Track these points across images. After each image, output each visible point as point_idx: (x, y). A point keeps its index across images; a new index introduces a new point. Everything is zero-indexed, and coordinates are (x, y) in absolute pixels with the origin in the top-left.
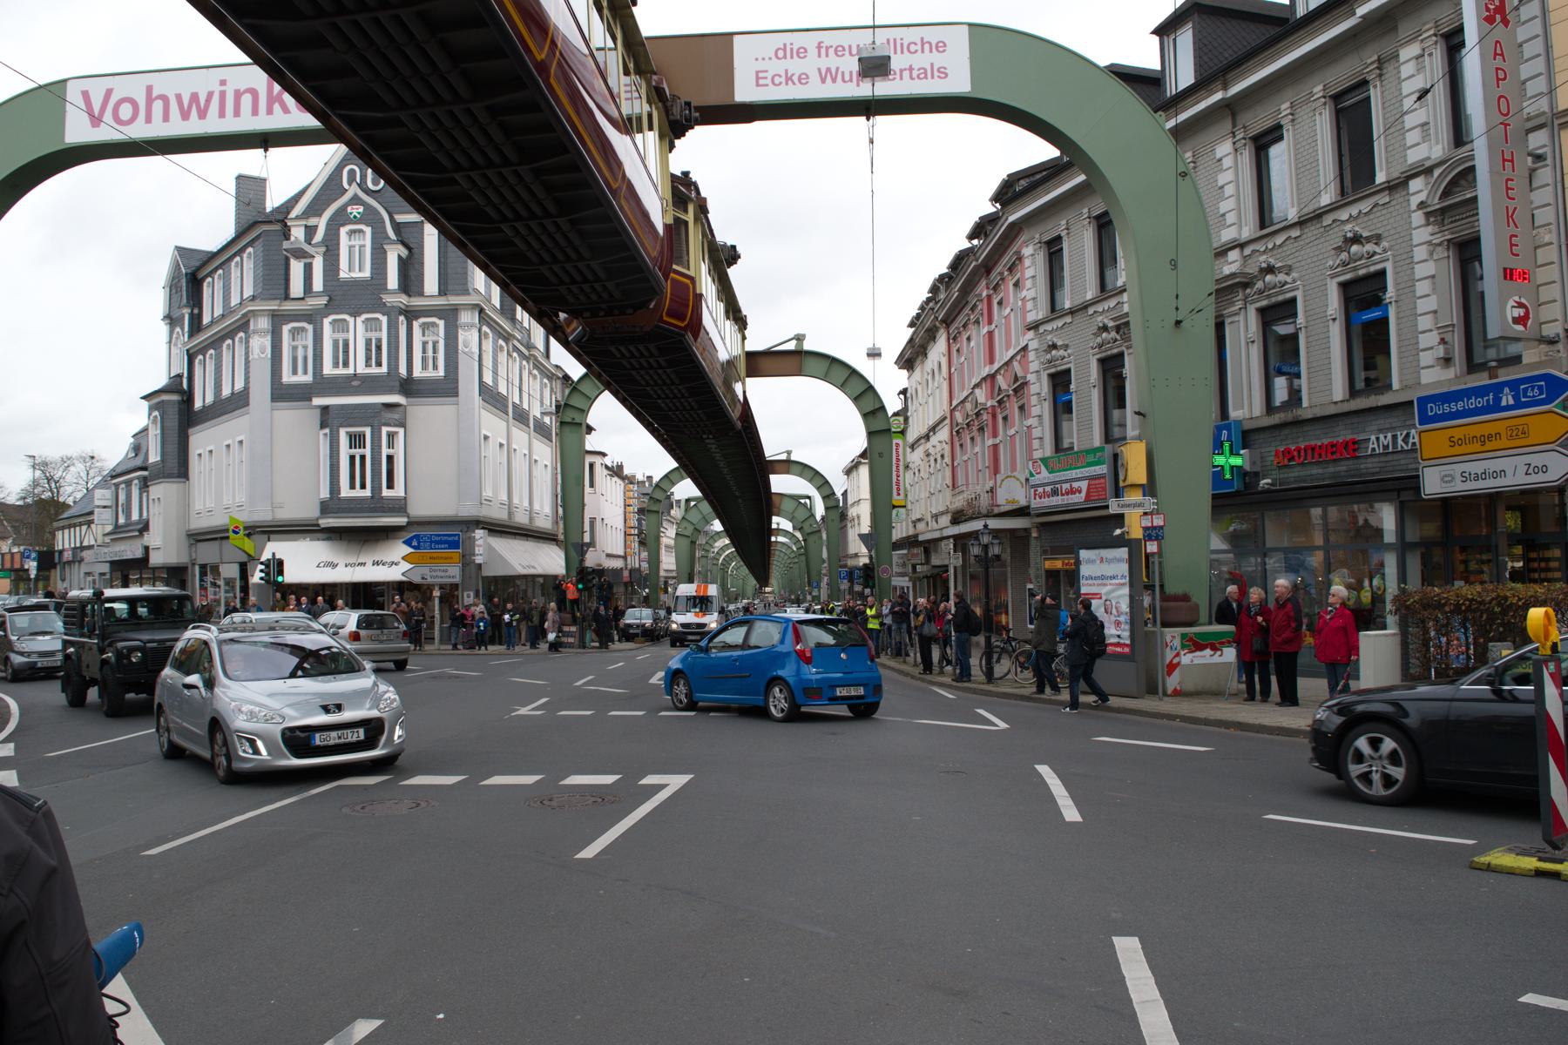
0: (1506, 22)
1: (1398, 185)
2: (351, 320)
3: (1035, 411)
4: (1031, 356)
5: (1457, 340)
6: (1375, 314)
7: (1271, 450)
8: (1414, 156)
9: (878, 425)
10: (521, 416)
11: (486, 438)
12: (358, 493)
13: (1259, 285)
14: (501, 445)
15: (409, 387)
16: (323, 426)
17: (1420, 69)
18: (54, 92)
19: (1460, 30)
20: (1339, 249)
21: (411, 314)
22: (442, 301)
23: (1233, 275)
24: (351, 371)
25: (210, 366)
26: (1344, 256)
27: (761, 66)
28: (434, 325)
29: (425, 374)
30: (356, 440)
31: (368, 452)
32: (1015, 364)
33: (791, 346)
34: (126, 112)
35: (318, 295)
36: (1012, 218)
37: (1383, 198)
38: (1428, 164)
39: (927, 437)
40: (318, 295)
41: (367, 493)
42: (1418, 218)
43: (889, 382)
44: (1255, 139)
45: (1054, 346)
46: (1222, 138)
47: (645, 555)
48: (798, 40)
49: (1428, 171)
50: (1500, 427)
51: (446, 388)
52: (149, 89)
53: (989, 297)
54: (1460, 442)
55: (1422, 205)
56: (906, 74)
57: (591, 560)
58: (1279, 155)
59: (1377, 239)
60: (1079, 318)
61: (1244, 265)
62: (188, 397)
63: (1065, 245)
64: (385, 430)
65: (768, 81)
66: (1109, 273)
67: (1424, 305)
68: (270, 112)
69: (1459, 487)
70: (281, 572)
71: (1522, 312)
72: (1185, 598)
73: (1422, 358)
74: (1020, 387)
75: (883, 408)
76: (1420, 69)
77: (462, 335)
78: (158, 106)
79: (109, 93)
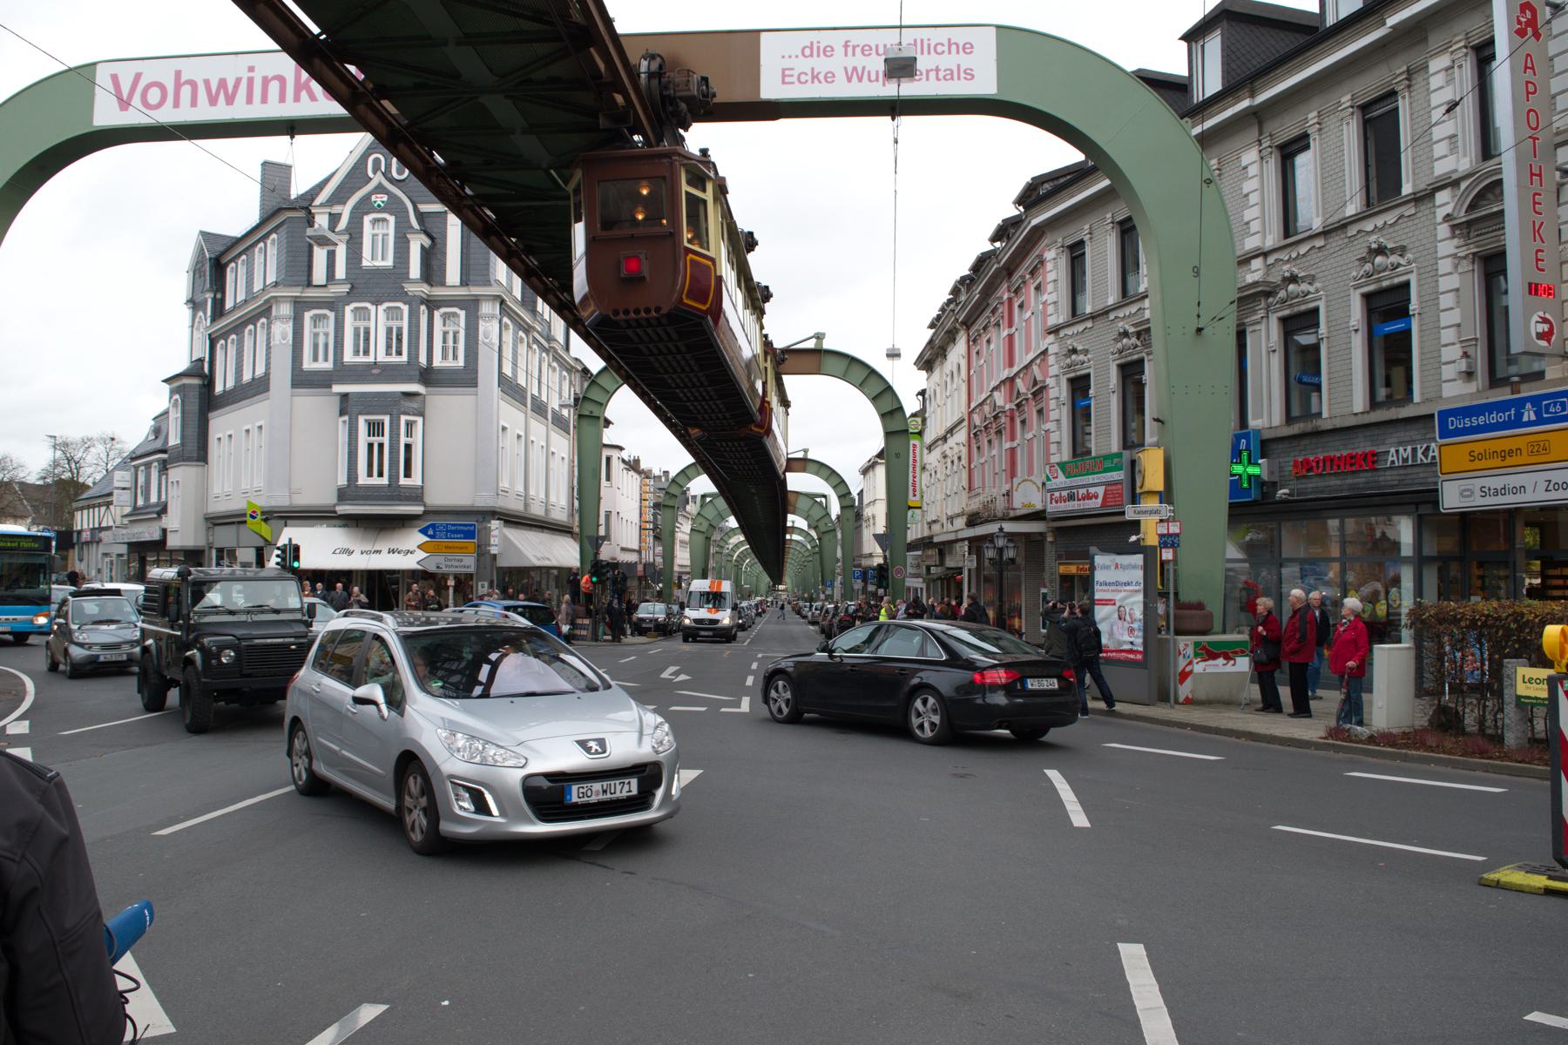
0: (1537, 36)
1: (1424, 197)
2: (372, 308)
3: (1053, 415)
4: (1051, 360)
5: (1480, 355)
6: (1397, 326)
7: (1288, 460)
8: (1440, 169)
9: (896, 425)
10: (539, 408)
11: (504, 429)
12: (375, 481)
13: (1282, 294)
14: (519, 437)
15: (429, 376)
16: (342, 413)
17: (1450, 81)
18: (83, 75)
19: (1490, 42)
20: (1363, 260)
21: (432, 304)
22: (463, 292)
23: (1255, 284)
24: (371, 359)
25: (232, 351)
26: (1368, 267)
27: (787, 63)
28: (455, 315)
29: (446, 364)
30: (375, 428)
31: (386, 440)
32: (1035, 367)
33: (811, 344)
34: (154, 96)
35: (341, 282)
36: (1035, 222)
37: (1409, 210)
38: (1455, 176)
39: (944, 439)
40: (341, 282)
41: (385, 481)
42: (1443, 230)
43: (907, 383)
44: (1281, 147)
45: (1074, 351)
46: (1248, 147)
47: (659, 549)
48: (825, 39)
49: (1455, 184)
50: (1521, 443)
51: (466, 378)
52: (178, 74)
53: (1010, 300)
54: (1481, 457)
55: (1448, 218)
56: (932, 75)
57: (606, 553)
58: (1304, 164)
59: (1402, 250)
60: (1100, 323)
61: (1267, 274)
62: (209, 381)
63: (1088, 250)
64: (403, 418)
65: (794, 79)
66: (1130, 279)
67: (1447, 319)
68: (297, 99)
69: (1478, 502)
70: (297, 558)
71: (1546, 327)
72: (1200, 606)
73: (1445, 370)
74: (1039, 391)
75: (901, 409)
76: (1450, 81)
77: (483, 326)
78: (186, 91)
79: (138, 76)
